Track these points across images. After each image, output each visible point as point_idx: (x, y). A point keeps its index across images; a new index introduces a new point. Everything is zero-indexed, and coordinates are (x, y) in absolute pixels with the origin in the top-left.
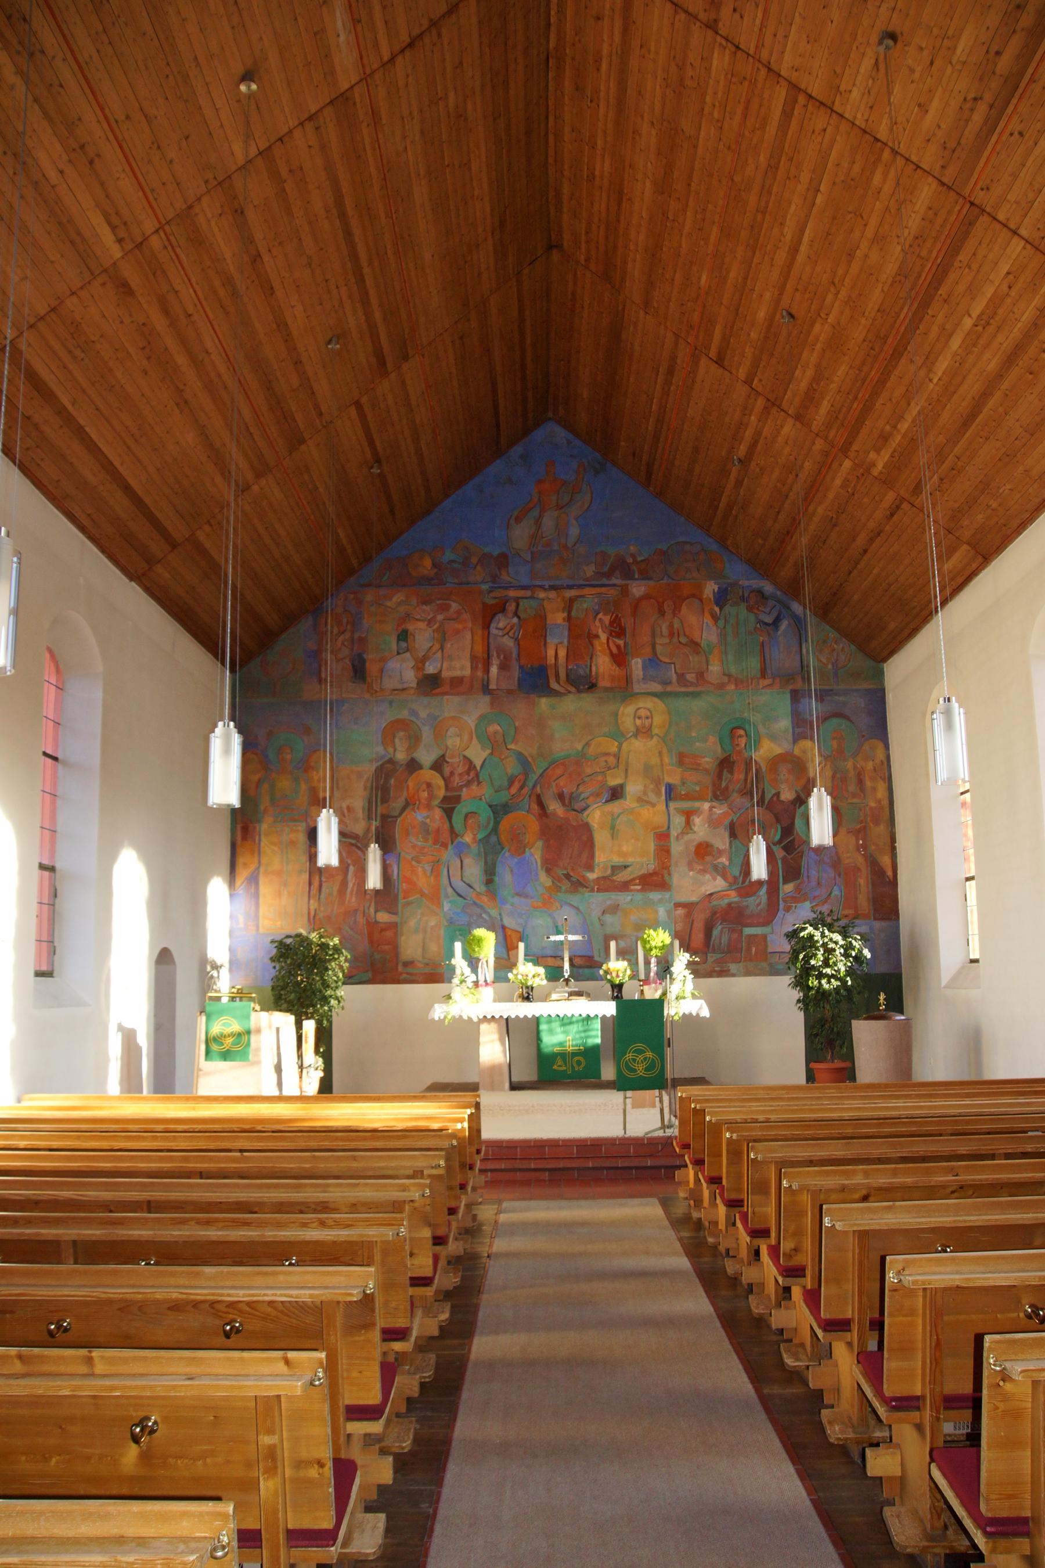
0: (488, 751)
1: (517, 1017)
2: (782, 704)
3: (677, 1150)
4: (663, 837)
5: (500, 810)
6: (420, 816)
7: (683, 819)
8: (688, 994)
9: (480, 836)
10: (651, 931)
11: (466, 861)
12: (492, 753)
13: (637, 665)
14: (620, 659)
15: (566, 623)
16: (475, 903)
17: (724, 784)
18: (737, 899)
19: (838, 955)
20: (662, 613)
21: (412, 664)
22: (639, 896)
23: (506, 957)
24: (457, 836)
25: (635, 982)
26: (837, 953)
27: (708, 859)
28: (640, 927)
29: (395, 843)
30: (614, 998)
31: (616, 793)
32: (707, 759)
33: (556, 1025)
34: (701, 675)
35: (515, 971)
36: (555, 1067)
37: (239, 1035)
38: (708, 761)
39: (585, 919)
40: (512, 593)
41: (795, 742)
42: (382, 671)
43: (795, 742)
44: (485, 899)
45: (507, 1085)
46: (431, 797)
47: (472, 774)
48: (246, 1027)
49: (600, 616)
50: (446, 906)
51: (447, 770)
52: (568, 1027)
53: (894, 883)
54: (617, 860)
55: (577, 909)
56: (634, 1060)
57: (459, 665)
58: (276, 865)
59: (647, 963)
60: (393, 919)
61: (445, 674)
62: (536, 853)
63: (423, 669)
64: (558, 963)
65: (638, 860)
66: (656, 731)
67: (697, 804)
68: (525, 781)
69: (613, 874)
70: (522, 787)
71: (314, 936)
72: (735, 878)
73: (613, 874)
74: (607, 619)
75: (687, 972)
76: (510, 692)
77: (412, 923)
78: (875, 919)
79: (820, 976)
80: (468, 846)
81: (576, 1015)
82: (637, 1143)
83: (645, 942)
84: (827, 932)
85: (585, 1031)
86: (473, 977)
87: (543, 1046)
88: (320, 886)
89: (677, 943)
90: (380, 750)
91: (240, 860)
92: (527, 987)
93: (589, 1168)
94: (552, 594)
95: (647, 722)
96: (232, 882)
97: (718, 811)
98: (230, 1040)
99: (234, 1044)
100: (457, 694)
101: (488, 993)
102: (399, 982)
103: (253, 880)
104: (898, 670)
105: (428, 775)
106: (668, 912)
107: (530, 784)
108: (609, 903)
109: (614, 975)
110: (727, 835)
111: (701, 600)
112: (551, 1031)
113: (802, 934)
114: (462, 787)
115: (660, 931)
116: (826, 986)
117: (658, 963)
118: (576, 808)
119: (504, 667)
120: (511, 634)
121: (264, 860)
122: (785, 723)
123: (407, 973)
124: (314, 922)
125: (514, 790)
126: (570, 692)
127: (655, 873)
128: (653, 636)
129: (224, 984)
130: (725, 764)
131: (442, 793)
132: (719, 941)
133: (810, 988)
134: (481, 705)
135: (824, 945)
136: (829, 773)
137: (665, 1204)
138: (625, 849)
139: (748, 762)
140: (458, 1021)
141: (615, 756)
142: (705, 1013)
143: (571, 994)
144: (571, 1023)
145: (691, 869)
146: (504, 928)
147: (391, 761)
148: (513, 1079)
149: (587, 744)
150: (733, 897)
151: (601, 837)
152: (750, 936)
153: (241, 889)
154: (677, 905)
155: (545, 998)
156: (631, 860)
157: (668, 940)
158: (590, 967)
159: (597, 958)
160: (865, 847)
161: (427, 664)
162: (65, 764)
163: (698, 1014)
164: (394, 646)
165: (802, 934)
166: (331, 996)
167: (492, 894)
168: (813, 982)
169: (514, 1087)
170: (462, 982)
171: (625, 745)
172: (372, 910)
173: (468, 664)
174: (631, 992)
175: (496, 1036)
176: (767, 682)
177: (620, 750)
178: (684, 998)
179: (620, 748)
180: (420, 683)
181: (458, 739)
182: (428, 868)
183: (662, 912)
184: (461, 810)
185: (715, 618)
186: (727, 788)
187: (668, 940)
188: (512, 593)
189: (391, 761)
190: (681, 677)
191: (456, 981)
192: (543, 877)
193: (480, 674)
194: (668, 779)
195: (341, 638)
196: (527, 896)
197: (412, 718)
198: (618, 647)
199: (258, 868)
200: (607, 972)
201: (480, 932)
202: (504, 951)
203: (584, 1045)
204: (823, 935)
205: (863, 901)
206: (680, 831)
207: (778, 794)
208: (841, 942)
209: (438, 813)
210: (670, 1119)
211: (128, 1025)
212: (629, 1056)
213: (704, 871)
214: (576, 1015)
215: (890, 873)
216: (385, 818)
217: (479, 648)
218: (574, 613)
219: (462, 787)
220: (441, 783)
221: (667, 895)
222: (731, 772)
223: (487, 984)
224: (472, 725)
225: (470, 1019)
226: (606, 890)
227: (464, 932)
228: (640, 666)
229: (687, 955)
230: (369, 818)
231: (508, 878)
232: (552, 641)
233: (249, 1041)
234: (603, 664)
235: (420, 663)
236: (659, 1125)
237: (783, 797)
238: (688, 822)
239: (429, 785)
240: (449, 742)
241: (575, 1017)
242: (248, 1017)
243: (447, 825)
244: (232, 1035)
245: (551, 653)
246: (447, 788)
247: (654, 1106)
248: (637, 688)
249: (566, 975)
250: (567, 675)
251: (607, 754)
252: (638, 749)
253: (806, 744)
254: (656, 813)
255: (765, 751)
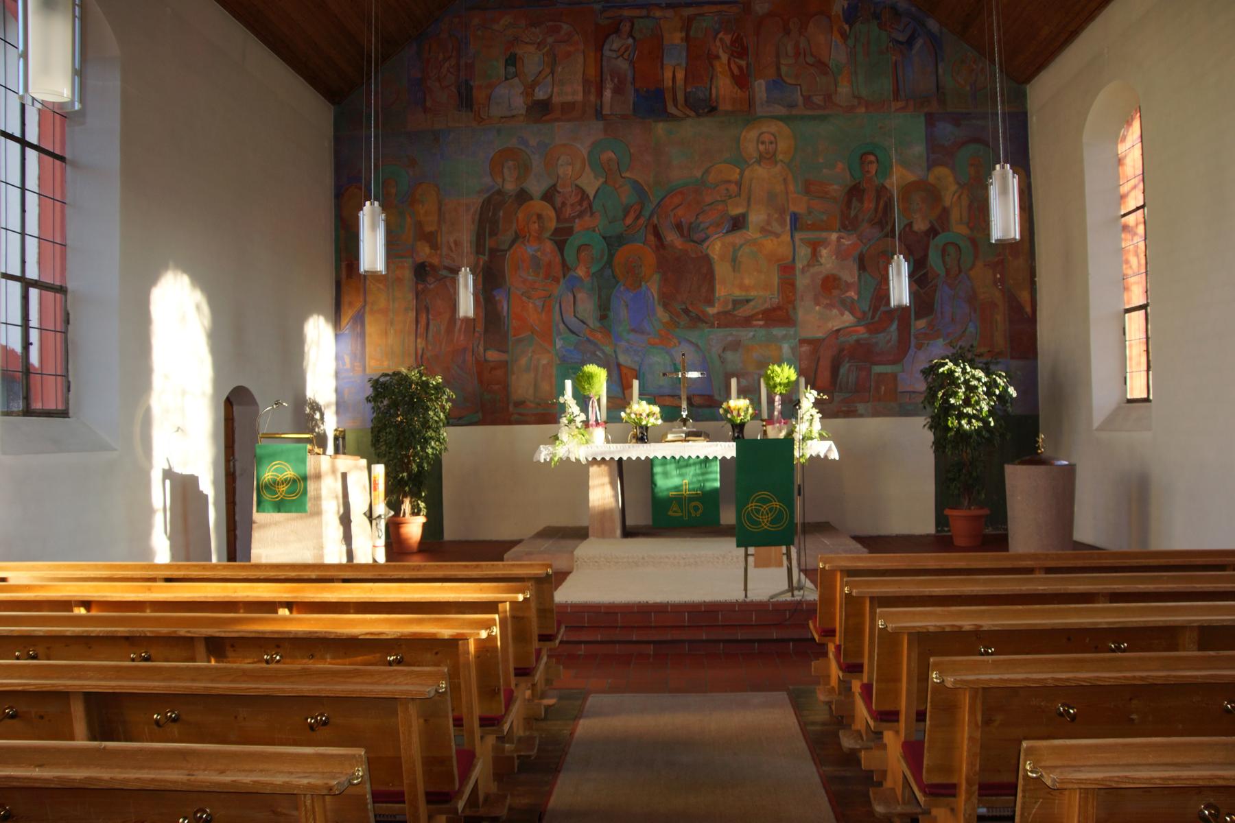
0: (602, 180)
1: (638, 458)
2: (916, 127)
3: (816, 637)
4: (787, 269)
5: (614, 242)
6: (530, 249)
7: (809, 250)
8: (815, 434)
9: (593, 270)
10: (776, 367)
11: (579, 296)
12: (606, 182)
13: (760, 87)
14: (742, 80)
15: (685, 44)
16: (589, 340)
17: (853, 213)
18: (866, 336)
19: (979, 391)
20: (787, 32)
21: (521, 89)
22: (762, 332)
23: (621, 395)
24: (569, 269)
25: (759, 423)
26: (980, 390)
27: (835, 292)
28: (763, 365)
29: (504, 277)
30: (734, 439)
31: (738, 223)
32: (835, 187)
33: (671, 468)
34: (828, 97)
35: (628, 411)
36: (670, 513)
37: (294, 481)
38: (836, 189)
39: (704, 357)
40: (626, 13)
41: (929, 168)
42: (489, 98)
43: (929, 168)
44: (599, 335)
45: (619, 532)
46: (542, 229)
47: (585, 204)
48: (302, 472)
49: (720, 35)
50: (559, 344)
51: (558, 200)
52: (684, 470)
53: (1032, 320)
54: (738, 293)
55: (697, 346)
56: (758, 511)
57: (571, 91)
58: (382, 303)
59: (771, 402)
60: (504, 357)
61: (555, 100)
62: (653, 287)
63: (533, 95)
64: (676, 402)
65: (761, 293)
66: (780, 157)
67: (824, 234)
68: (642, 209)
69: (734, 309)
70: (637, 218)
71: (414, 375)
72: (864, 313)
73: (734, 309)
74: (728, 39)
75: (814, 411)
76: (624, 117)
77: (524, 361)
78: (1012, 358)
79: (961, 416)
80: (580, 279)
81: (694, 457)
82: (759, 607)
83: (769, 378)
84: (968, 369)
85: (703, 474)
86: (583, 417)
87: (656, 490)
88: (428, 325)
89: (802, 380)
90: (488, 180)
91: (346, 299)
92: (641, 427)
93: (702, 641)
94: (669, 13)
95: (771, 147)
96: (337, 322)
97: (846, 242)
98: (284, 488)
99: (289, 492)
100: (569, 120)
101: (599, 433)
102: (510, 423)
103: (359, 319)
104: (1044, 90)
105: (538, 205)
106: (793, 349)
107: (646, 213)
108: (730, 338)
109: (735, 413)
110: (856, 267)
111: (829, 17)
112: (666, 475)
113: (941, 370)
114: (574, 218)
115: (786, 367)
116: (967, 427)
117: (783, 403)
118: (695, 239)
119: (618, 91)
120: (626, 56)
121: (369, 299)
122: (919, 149)
123: (520, 414)
124: (421, 360)
125: (629, 221)
126: (688, 116)
127: (779, 308)
128: (778, 56)
129: (330, 425)
130: (855, 192)
131: (553, 225)
132: (847, 384)
133: (948, 429)
134: (595, 130)
135: (966, 382)
136: (965, 202)
137: (799, 703)
138: (747, 282)
139: (881, 191)
140: (566, 463)
141: (736, 183)
142: (835, 455)
143: (688, 434)
144: (687, 465)
145: (818, 304)
146: (619, 365)
147: (499, 192)
148: (628, 523)
149: (707, 172)
150: (862, 334)
151: (722, 270)
152: (879, 374)
153: (346, 330)
154: (803, 341)
155: (661, 439)
156: (753, 293)
157: (793, 377)
158: (710, 406)
159: (717, 397)
160: (1002, 281)
161: (537, 89)
162: (75, 165)
163: (826, 457)
164: (502, 72)
165: (941, 370)
166: (431, 438)
167: (607, 330)
168: (952, 422)
169: (628, 533)
170: (571, 421)
171: (746, 173)
172: (481, 349)
173: (581, 88)
174: (753, 431)
175: (606, 480)
176: (900, 104)
177: (742, 177)
178: (812, 439)
179: (742, 174)
180: (529, 109)
181: (570, 168)
182: (539, 303)
183: (786, 348)
184: (573, 242)
185: (844, 36)
186: (856, 216)
187: (793, 377)
188: (626, 13)
189: (499, 192)
190: (807, 100)
191: (564, 420)
192: (661, 314)
193: (592, 98)
194: (793, 209)
195: (447, 65)
196: (643, 333)
197: (522, 147)
198: (740, 68)
199: (364, 307)
200: (728, 410)
201: (591, 368)
202: (619, 390)
203: (702, 488)
204: (964, 372)
205: (1000, 340)
206: (805, 263)
207: (910, 225)
208: (984, 379)
209: (549, 246)
210: (799, 580)
211: (180, 469)
212: (752, 506)
213: (830, 306)
214: (694, 457)
215: (1028, 309)
216: (493, 252)
217: (592, 72)
218: (692, 33)
219: (574, 218)
220: (553, 214)
221: (792, 331)
222: (861, 201)
223: (597, 423)
224: (585, 152)
225: (578, 461)
226: (726, 326)
227: (573, 369)
228: (763, 88)
229: (815, 393)
230: (478, 252)
231: (624, 313)
232: (669, 62)
233: (305, 488)
234: (723, 86)
235: (530, 88)
236: (786, 587)
237: (916, 227)
238: (815, 254)
239: (539, 217)
240: (561, 171)
241: (692, 457)
242: (304, 461)
243: (558, 259)
244: (286, 481)
245: (668, 75)
246: (558, 220)
247: (780, 565)
248: (760, 111)
249: (684, 414)
250: (686, 101)
251: (729, 182)
252: (761, 173)
253: (941, 171)
254: (779, 245)
255: (896, 179)
